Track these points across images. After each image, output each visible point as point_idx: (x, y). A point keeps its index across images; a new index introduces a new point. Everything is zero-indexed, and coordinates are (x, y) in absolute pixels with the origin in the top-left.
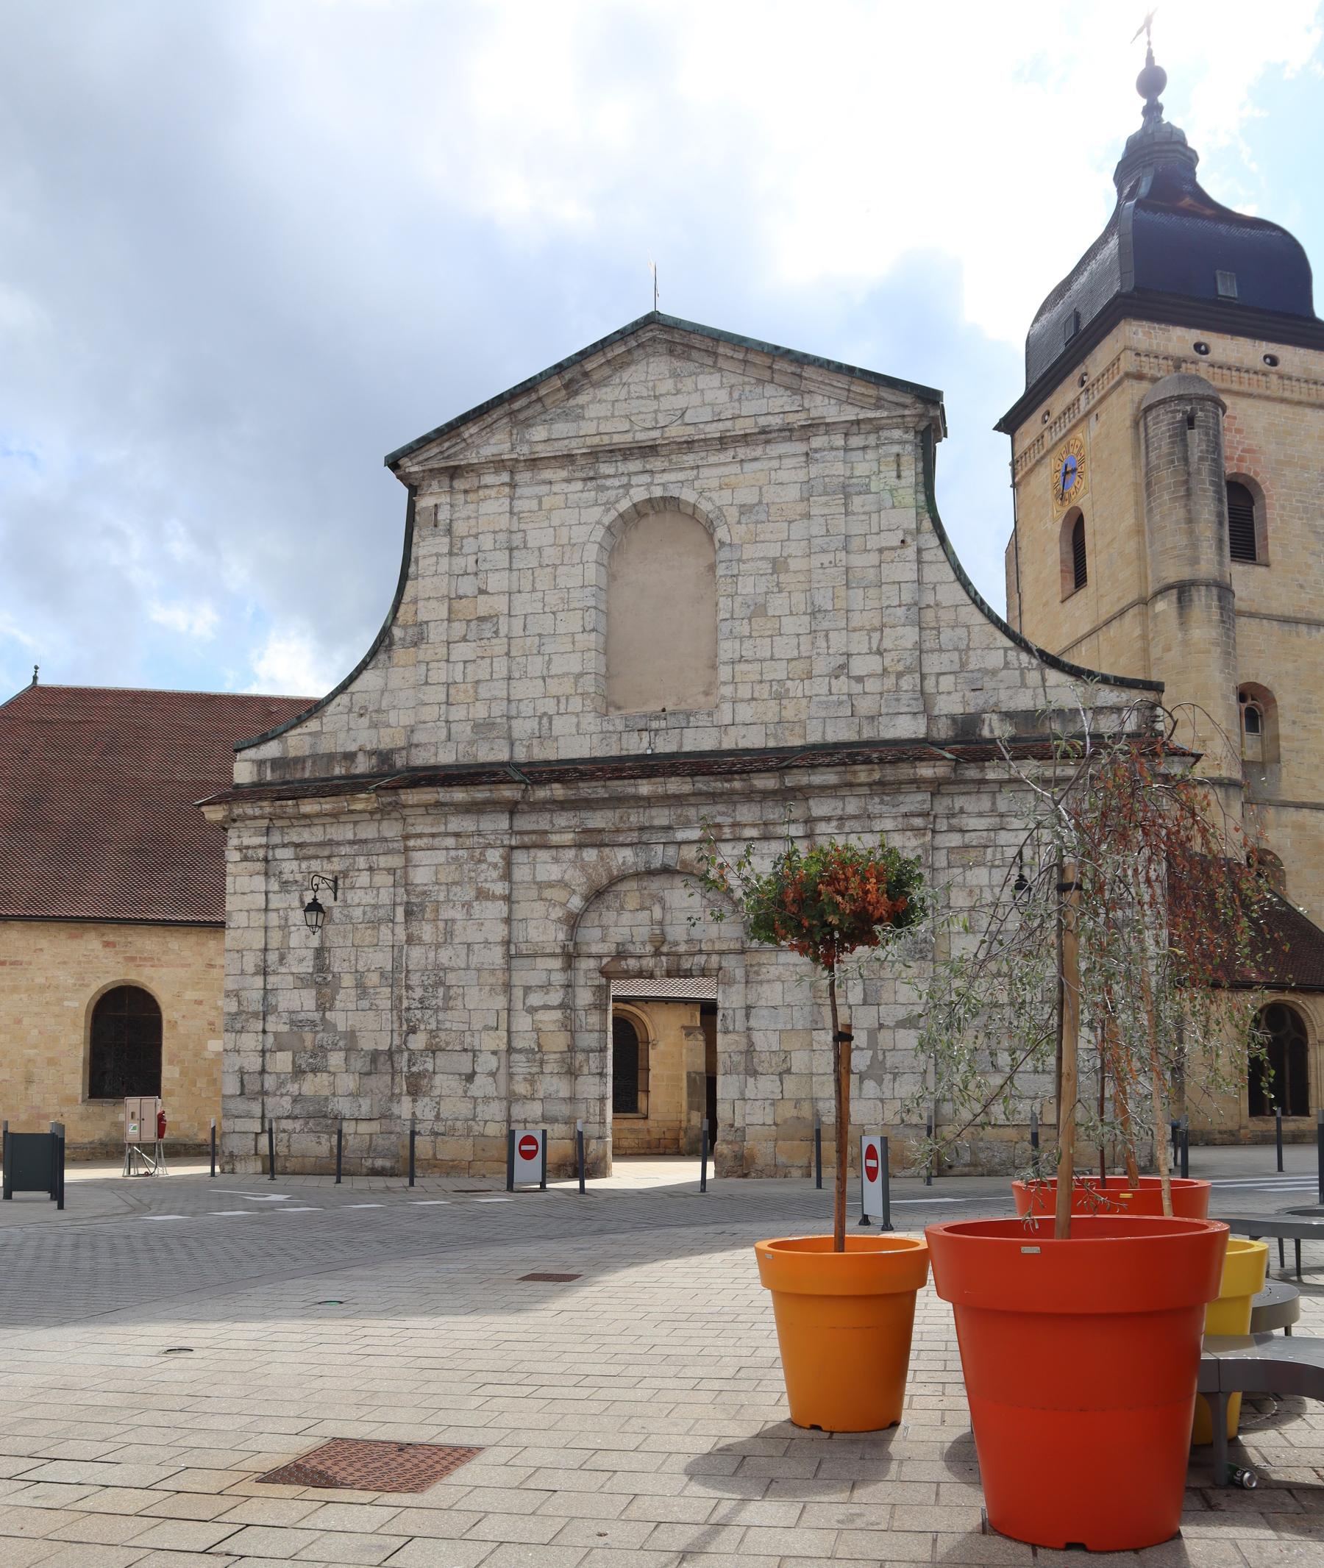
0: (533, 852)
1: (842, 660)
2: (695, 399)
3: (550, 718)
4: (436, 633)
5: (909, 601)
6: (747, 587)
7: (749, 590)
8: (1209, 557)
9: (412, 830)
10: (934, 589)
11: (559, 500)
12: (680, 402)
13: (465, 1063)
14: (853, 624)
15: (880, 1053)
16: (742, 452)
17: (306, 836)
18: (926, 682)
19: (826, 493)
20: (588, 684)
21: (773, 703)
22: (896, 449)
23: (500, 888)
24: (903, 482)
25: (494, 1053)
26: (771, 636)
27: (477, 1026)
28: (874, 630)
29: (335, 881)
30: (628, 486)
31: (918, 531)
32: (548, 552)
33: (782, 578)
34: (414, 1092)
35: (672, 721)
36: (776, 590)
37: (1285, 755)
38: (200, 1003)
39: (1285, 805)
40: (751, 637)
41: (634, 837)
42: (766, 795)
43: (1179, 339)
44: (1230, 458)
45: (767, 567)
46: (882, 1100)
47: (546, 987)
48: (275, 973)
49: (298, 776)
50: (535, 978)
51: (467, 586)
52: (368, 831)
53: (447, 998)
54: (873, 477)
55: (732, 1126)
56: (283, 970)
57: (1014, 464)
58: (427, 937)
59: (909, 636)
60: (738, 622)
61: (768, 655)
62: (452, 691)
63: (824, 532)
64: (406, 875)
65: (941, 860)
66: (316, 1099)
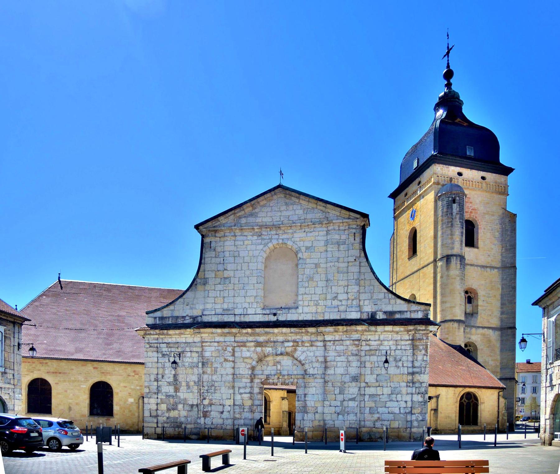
0: (241, 348)
1: (335, 295)
3: (247, 309)
6: (307, 271)
11: (250, 242)
13: (220, 409)
14: (339, 284)
19: (332, 244)
21: (314, 307)
22: (354, 231)
23: (231, 359)
24: (356, 242)
25: (230, 406)
27: (224, 398)
28: (345, 286)
29: (180, 354)
31: (360, 256)
32: (246, 258)
34: (205, 416)
37: (480, 311)
38: (126, 387)
39: (479, 327)
45: (313, 266)
47: (245, 387)
49: (167, 323)
50: (241, 385)
51: (221, 267)
53: (215, 390)
56: (163, 380)
57: (394, 210)
58: (208, 372)
62: (216, 299)
64: (202, 354)
65: (363, 353)
66: (174, 418)
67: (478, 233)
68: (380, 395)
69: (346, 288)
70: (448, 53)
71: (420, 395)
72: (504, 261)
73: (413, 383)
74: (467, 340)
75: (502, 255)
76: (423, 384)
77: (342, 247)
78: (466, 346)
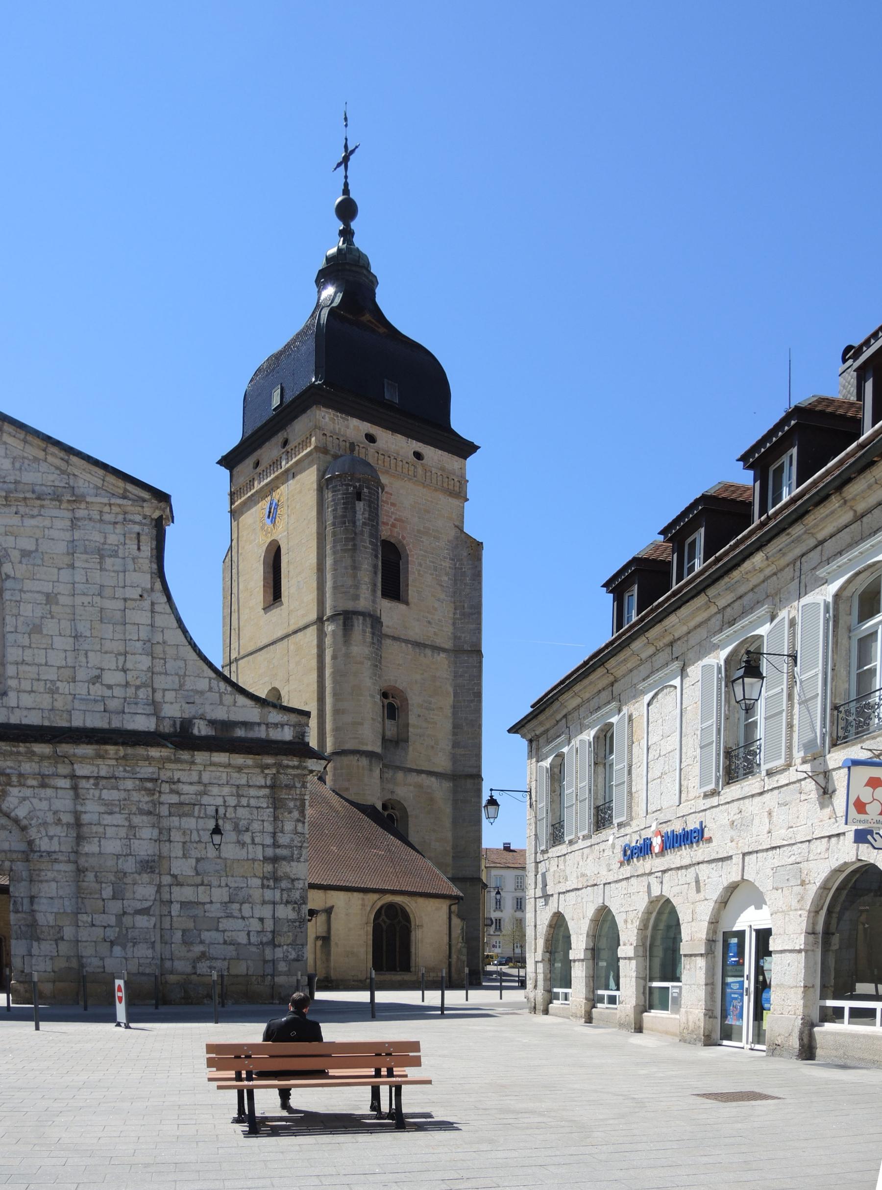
1: (97, 672)
5: (146, 638)
6: (27, 610)
10: (162, 631)
15: (124, 929)
18: (156, 694)
19: (86, 552)
21: (47, 696)
24: (142, 554)
26: (46, 649)
28: (120, 654)
31: (152, 589)
33: (54, 608)
36: (49, 616)
37: (412, 737)
39: (411, 770)
40: (30, 647)
42: (43, 757)
43: (355, 428)
45: (41, 598)
46: (126, 959)
54: (121, 547)
55: (23, 972)
57: (232, 494)
59: (145, 662)
60: (20, 636)
61: (43, 662)
63: (84, 580)
65: (164, 810)
68: (204, 904)
71: (290, 907)
72: (460, 638)
74: (389, 796)
75: (454, 624)
76: (296, 883)
77: (109, 561)
78: (385, 807)
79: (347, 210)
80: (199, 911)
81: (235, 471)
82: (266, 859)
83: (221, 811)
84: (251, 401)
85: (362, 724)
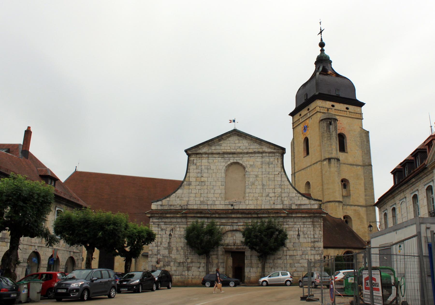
2: (242, 145)
4: (193, 184)
7: (252, 180)
8: (335, 152)
9: (188, 221)
11: (217, 161)
12: (239, 145)
16: (251, 155)
17: (166, 220)
20: (223, 195)
22: (277, 157)
30: (229, 159)
32: (215, 170)
34: (188, 270)
35: (237, 203)
39: (351, 205)
41: (231, 224)
44: (339, 130)
48: (160, 246)
52: (179, 220)
57: (293, 123)
67: (346, 143)
68: (295, 256)
69: (274, 190)
70: (321, 32)
72: (364, 161)
73: (315, 248)
77: (271, 165)
78: (344, 218)
79: (322, 45)
80: (294, 258)
81: (294, 117)
82: (311, 242)
83: (299, 229)
84: (298, 97)
85: (335, 192)
